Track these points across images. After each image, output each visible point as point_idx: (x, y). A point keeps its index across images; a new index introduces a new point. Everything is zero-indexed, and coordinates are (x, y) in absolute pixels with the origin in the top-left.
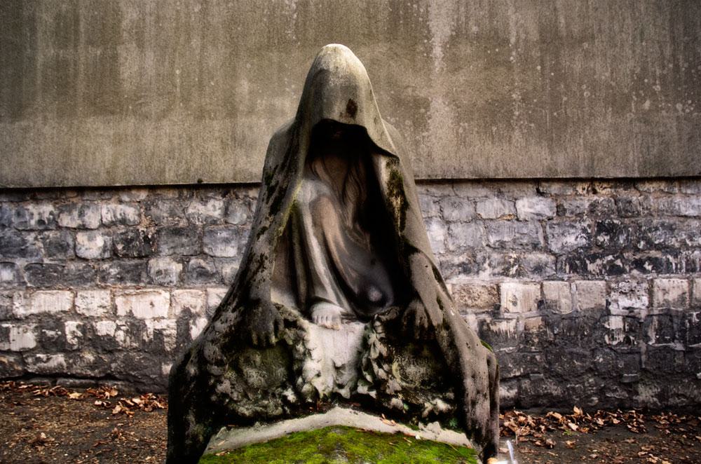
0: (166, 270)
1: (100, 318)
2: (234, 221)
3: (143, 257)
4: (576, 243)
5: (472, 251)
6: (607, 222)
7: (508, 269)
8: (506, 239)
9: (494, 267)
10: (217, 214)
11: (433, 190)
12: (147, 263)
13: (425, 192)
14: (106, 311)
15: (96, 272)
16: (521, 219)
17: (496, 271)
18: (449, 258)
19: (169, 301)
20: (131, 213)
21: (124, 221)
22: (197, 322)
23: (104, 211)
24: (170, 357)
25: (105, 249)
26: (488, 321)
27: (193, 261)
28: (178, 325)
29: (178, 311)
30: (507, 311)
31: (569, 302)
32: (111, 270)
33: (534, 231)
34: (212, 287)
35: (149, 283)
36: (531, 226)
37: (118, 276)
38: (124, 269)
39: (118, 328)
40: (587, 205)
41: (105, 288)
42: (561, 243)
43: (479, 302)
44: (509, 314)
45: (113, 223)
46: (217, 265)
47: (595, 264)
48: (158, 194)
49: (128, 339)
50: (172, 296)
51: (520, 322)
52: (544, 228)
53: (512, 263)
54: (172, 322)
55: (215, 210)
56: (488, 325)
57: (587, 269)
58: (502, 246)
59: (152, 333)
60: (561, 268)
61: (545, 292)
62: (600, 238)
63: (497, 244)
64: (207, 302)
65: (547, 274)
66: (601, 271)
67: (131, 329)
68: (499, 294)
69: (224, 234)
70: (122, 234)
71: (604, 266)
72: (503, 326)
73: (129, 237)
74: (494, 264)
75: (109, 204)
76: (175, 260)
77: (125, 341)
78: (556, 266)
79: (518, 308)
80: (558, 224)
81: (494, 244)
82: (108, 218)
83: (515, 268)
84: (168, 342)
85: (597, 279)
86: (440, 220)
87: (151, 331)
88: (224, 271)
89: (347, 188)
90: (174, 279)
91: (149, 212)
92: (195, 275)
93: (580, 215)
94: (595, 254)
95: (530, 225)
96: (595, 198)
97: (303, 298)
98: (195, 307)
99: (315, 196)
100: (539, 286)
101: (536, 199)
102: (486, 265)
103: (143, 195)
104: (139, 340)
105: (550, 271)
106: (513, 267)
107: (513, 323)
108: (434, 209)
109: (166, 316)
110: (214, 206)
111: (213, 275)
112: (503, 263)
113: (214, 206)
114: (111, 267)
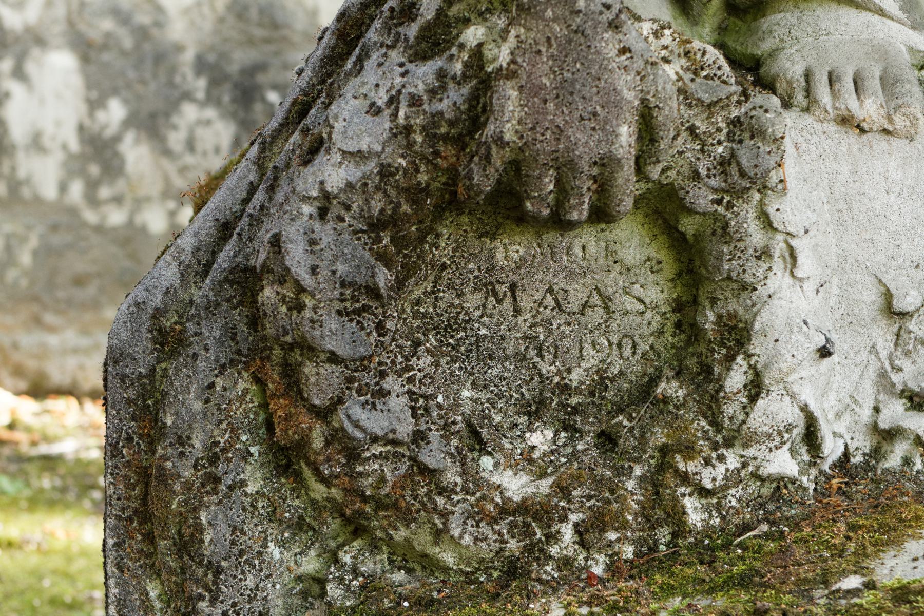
22: (30, 67)
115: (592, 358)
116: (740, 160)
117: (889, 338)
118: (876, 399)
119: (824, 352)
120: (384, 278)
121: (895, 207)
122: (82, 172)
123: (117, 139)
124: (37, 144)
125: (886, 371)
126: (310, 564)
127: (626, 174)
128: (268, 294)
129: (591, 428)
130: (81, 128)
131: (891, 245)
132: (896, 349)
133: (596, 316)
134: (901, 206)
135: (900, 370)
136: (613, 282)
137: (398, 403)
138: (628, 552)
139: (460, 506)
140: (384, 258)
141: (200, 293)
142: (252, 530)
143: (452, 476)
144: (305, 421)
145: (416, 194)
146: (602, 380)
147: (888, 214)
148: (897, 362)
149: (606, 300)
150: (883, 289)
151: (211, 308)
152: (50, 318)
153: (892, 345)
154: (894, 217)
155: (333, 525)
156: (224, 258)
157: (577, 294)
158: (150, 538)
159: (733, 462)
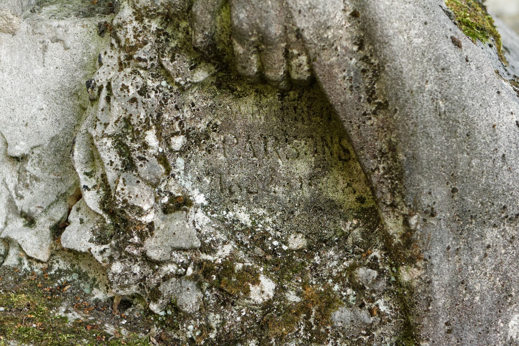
116: (233, 11)
117: (14, 175)
118: (7, 217)
121: (8, 82)
125: (12, 198)
131: (9, 109)
132: (19, 183)
134: (12, 81)
135: (22, 197)
147: (4, 87)
148: (20, 192)
150: (4, 140)
153: (17, 180)
154: (9, 89)
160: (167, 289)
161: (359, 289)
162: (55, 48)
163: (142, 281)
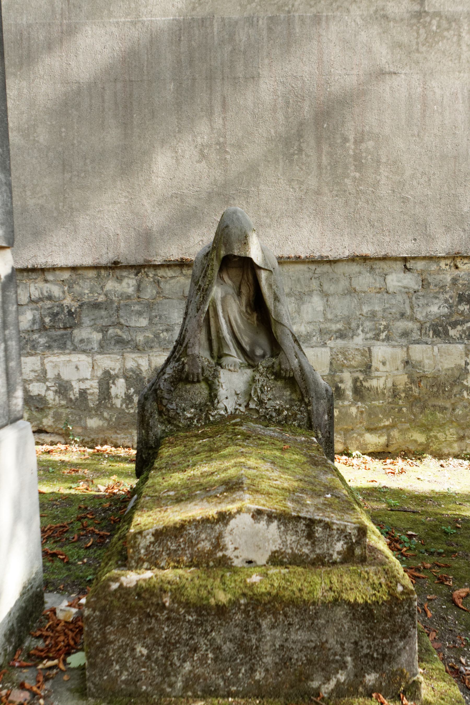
0: (88, 339)
1: (31, 381)
2: (146, 295)
3: (68, 328)
4: (439, 311)
5: (347, 320)
6: (467, 293)
7: (378, 335)
8: (377, 308)
9: (367, 333)
10: (131, 290)
11: (313, 267)
12: (71, 333)
13: (307, 270)
14: (36, 375)
15: (27, 341)
16: (390, 292)
17: (368, 336)
18: (328, 325)
19: (91, 365)
20: (56, 291)
21: (50, 298)
22: (116, 382)
23: (32, 289)
24: (93, 412)
25: (34, 322)
26: (361, 379)
27: (111, 331)
28: (99, 385)
29: (99, 373)
30: (377, 370)
31: (431, 362)
32: (40, 340)
33: (402, 301)
34: (128, 352)
35: (74, 350)
36: (399, 298)
37: (46, 344)
38: (52, 338)
39: (48, 389)
40: (449, 278)
41: (36, 354)
42: (425, 312)
43: (353, 363)
44: (379, 373)
45: (41, 299)
46: (132, 333)
47: (456, 330)
48: (80, 274)
49: (57, 398)
50: (94, 361)
51: (389, 379)
52: (410, 298)
53: (382, 329)
54: (95, 383)
55: (129, 288)
56: (361, 382)
57: (448, 334)
58: (373, 315)
59: (78, 392)
60: (426, 333)
61: (410, 354)
62: (461, 308)
63: (369, 313)
64: (124, 365)
65: (413, 339)
66: (461, 336)
67: (60, 390)
68: (370, 356)
69: (137, 308)
70: (49, 308)
71: (464, 332)
72: (374, 383)
73: (55, 311)
74: (366, 330)
75: (36, 283)
76: (95, 330)
77: (54, 400)
78: (421, 332)
79: (387, 368)
80: (423, 296)
81: (367, 313)
82: (35, 294)
83: (384, 334)
84: (91, 400)
85: (457, 343)
86: (319, 293)
87: (76, 390)
88: (138, 339)
89: (242, 287)
90: (96, 346)
91: (72, 290)
92: (113, 342)
93: (443, 287)
94: (456, 321)
95: (398, 296)
96: (457, 272)
97: (215, 354)
98: (114, 370)
99: (224, 294)
100: (405, 349)
101: (402, 275)
102: (360, 331)
103: (66, 275)
104: (66, 398)
105: (415, 335)
106: (383, 332)
107: (382, 381)
108: (315, 284)
109: (89, 378)
110: (128, 284)
111: (128, 342)
112: (375, 330)
113: (128, 284)
114: (40, 337)
115: (199, 400)
119: (227, 398)
120: (172, 389)
122: (125, 402)
123: (132, 396)
124: (117, 397)
126: (164, 428)
127: (200, 375)
128: (158, 392)
129: (199, 409)
130: (125, 393)
133: (199, 395)
136: (201, 390)
137: (174, 405)
138: (203, 423)
139: (182, 418)
140: (172, 386)
141: (150, 392)
142: (156, 423)
143: (181, 414)
144: (163, 407)
145: (176, 378)
146: (200, 403)
149: (201, 393)
151: (151, 394)
152: (118, 432)
155: (166, 422)
156: (153, 388)
157: (197, 392)
158: (143, 424)
159: (216, 412)
160: (270, 413)
161: (301, 411)
162: (245, 375)
163: (265, 412)
